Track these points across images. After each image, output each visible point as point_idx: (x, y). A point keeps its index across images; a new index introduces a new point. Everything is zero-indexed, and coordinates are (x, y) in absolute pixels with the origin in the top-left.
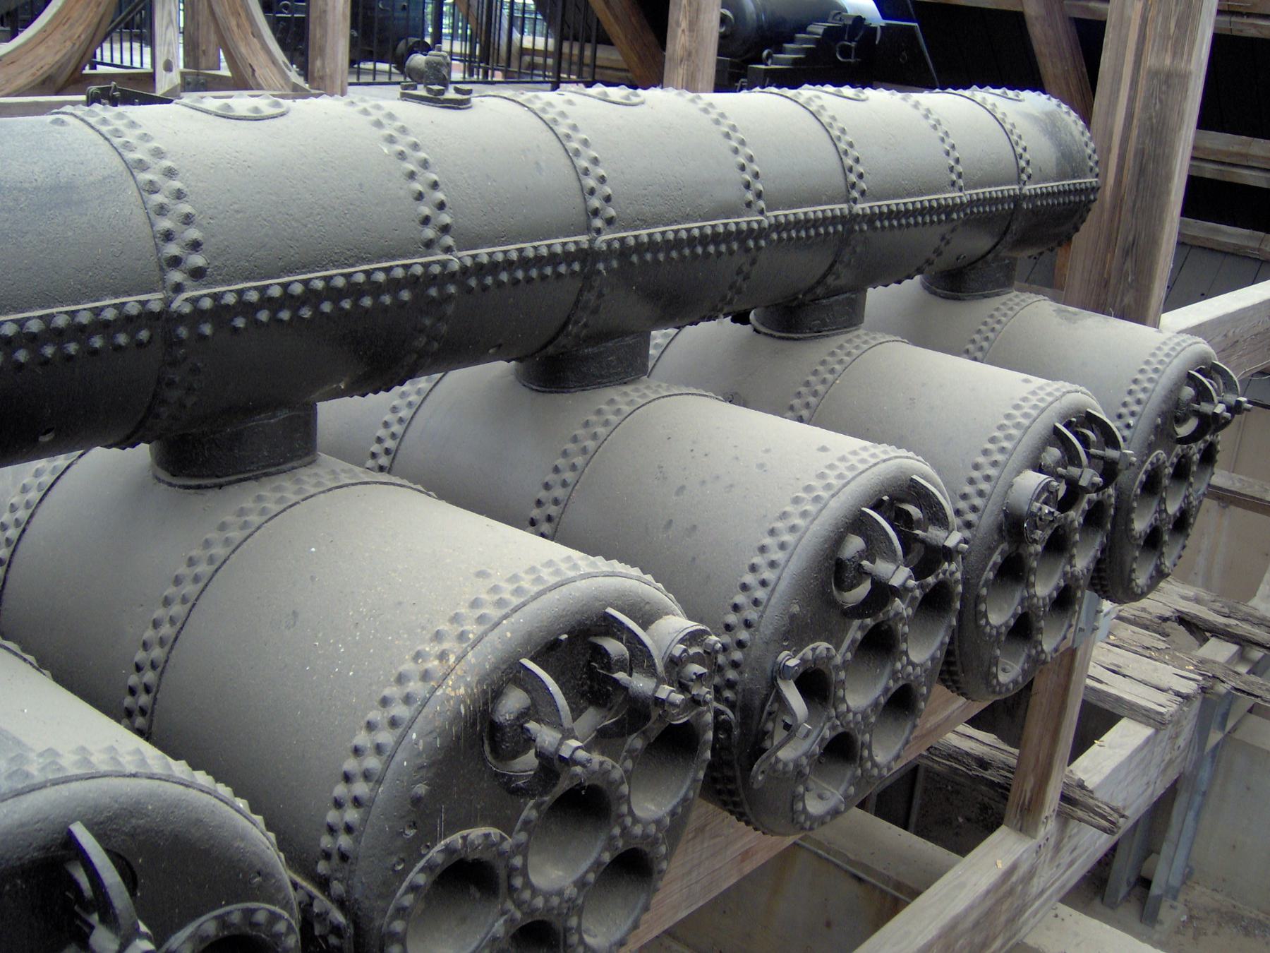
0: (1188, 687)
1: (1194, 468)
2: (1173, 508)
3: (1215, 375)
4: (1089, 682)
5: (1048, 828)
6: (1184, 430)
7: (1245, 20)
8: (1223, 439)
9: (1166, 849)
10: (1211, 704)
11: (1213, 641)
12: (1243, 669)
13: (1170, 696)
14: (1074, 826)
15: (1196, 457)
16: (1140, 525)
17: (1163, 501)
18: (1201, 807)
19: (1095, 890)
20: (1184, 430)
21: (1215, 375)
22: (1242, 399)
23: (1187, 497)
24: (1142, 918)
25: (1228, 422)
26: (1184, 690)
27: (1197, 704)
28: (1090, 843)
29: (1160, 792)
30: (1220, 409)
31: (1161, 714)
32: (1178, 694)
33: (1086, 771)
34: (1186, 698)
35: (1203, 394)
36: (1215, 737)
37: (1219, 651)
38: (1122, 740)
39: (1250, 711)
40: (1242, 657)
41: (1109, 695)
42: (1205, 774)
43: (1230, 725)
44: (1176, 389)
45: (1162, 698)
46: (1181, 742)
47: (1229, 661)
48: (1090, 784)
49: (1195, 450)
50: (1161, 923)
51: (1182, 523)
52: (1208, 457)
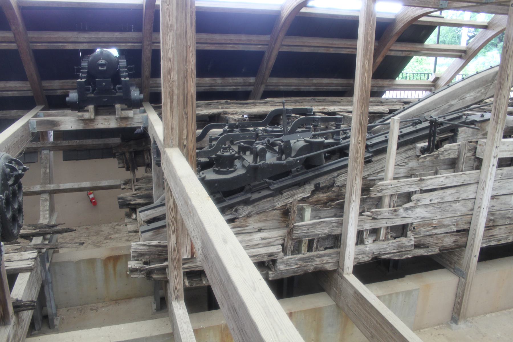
0: (35, 255)
1: (17, 192)
2: (16, 206)
3: (475, 123)
4: (6, 268)
5: (13, 319)
6: (10, 182)
7: (228, 45)
8: (22, 180)
9: (48, 304)
10: (43, 258)
11: (34, 238)
12: (47, 242)
13: (30, 260)
14: (21, 314)
15: (17, 189)
16: (9, 215)
17: (12, 205)
18: (52, 287)
19: (33, 329)
20: (10, 182)
21: (475, 123)
22: (25, 166)
23: (18, 201)
24: (50, 328)
25: (23, 175)
26: (34, 257)
27: (39, 259)
28: (27, 315)
29: (39, 289)
30: (20, 172)
31: (30, 267)
32: (32, 259)
33: (16, 295)
34: (35, 258)
35: (13, 169)
36: (48, 265)
37: (37, 240)
38: (22, 282)
39: (53, 253)
40: (45, 239)
41: (11, 269)
42: (49, 277)
43: (50, 259)
44: (4, 171)
45: (28, 262)
46: (39, 271)
47: (42, 242)
48: (20, 299)
49: (16, 187)
50: (56, 325)
51: (20, 210)
52: (20, 187)
